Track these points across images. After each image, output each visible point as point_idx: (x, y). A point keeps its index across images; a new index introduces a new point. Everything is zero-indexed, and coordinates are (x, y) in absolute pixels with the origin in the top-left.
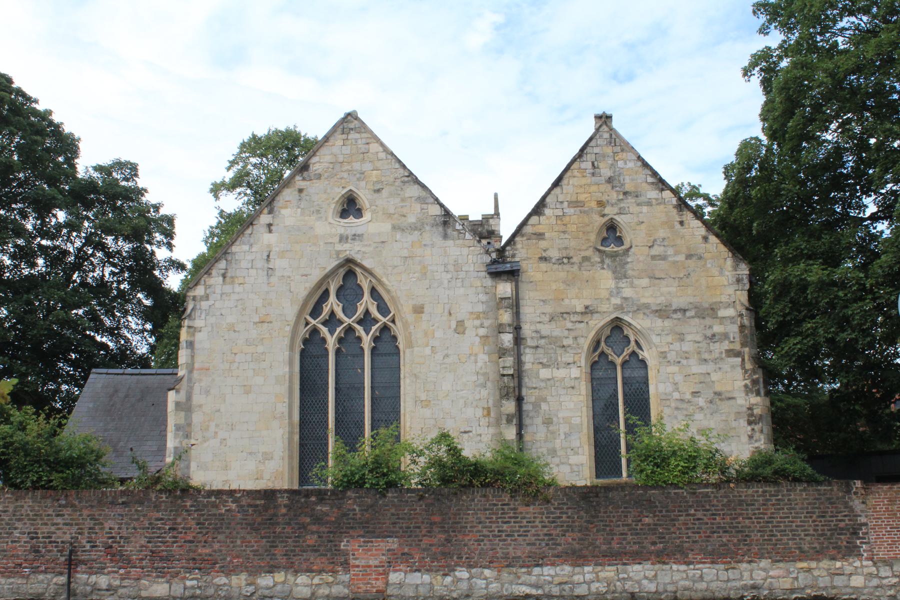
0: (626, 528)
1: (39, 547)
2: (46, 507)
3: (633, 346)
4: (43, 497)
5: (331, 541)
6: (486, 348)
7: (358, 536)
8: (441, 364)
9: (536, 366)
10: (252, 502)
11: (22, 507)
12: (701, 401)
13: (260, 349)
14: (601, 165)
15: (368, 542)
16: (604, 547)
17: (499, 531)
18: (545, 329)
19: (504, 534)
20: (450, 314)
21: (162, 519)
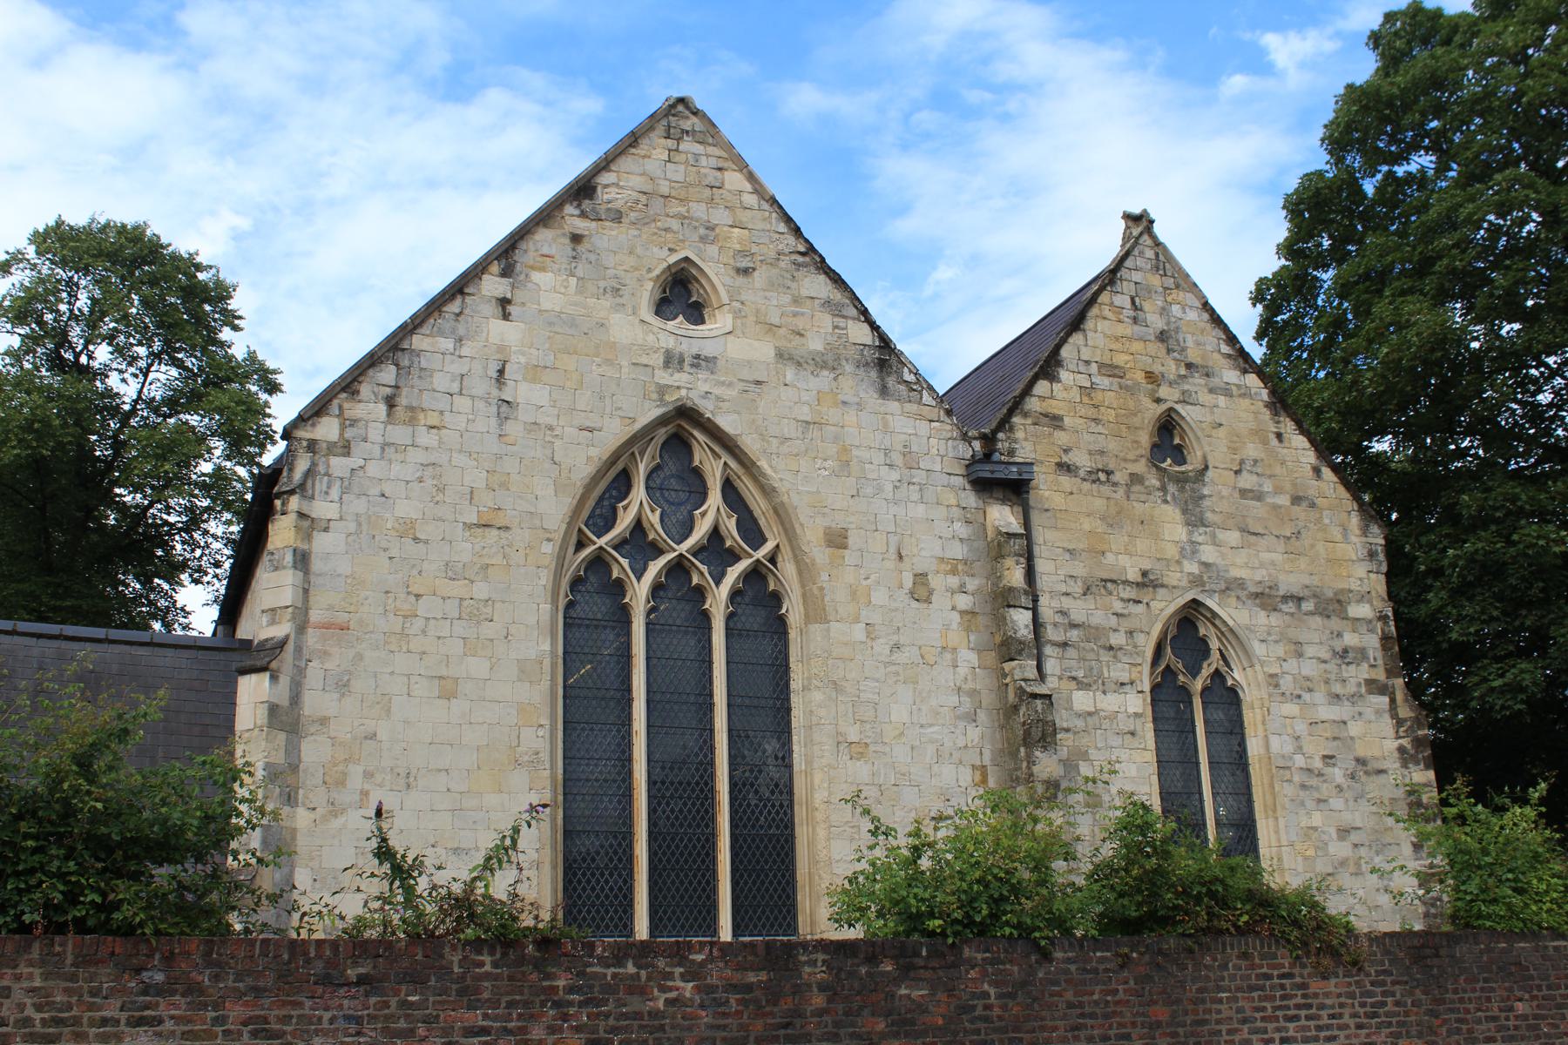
0: (1492, 1025)
2: (94, 993)
3: (1214, 662)
4: (83, 961)
6: (972, 638)
8: (887, 664)
9: (1067, 685)
10: (737, 977)
12: (1338, 774)
13: (481, 590)
14: (1147, 306)
18: (1080, 609)
20: (901, 557)
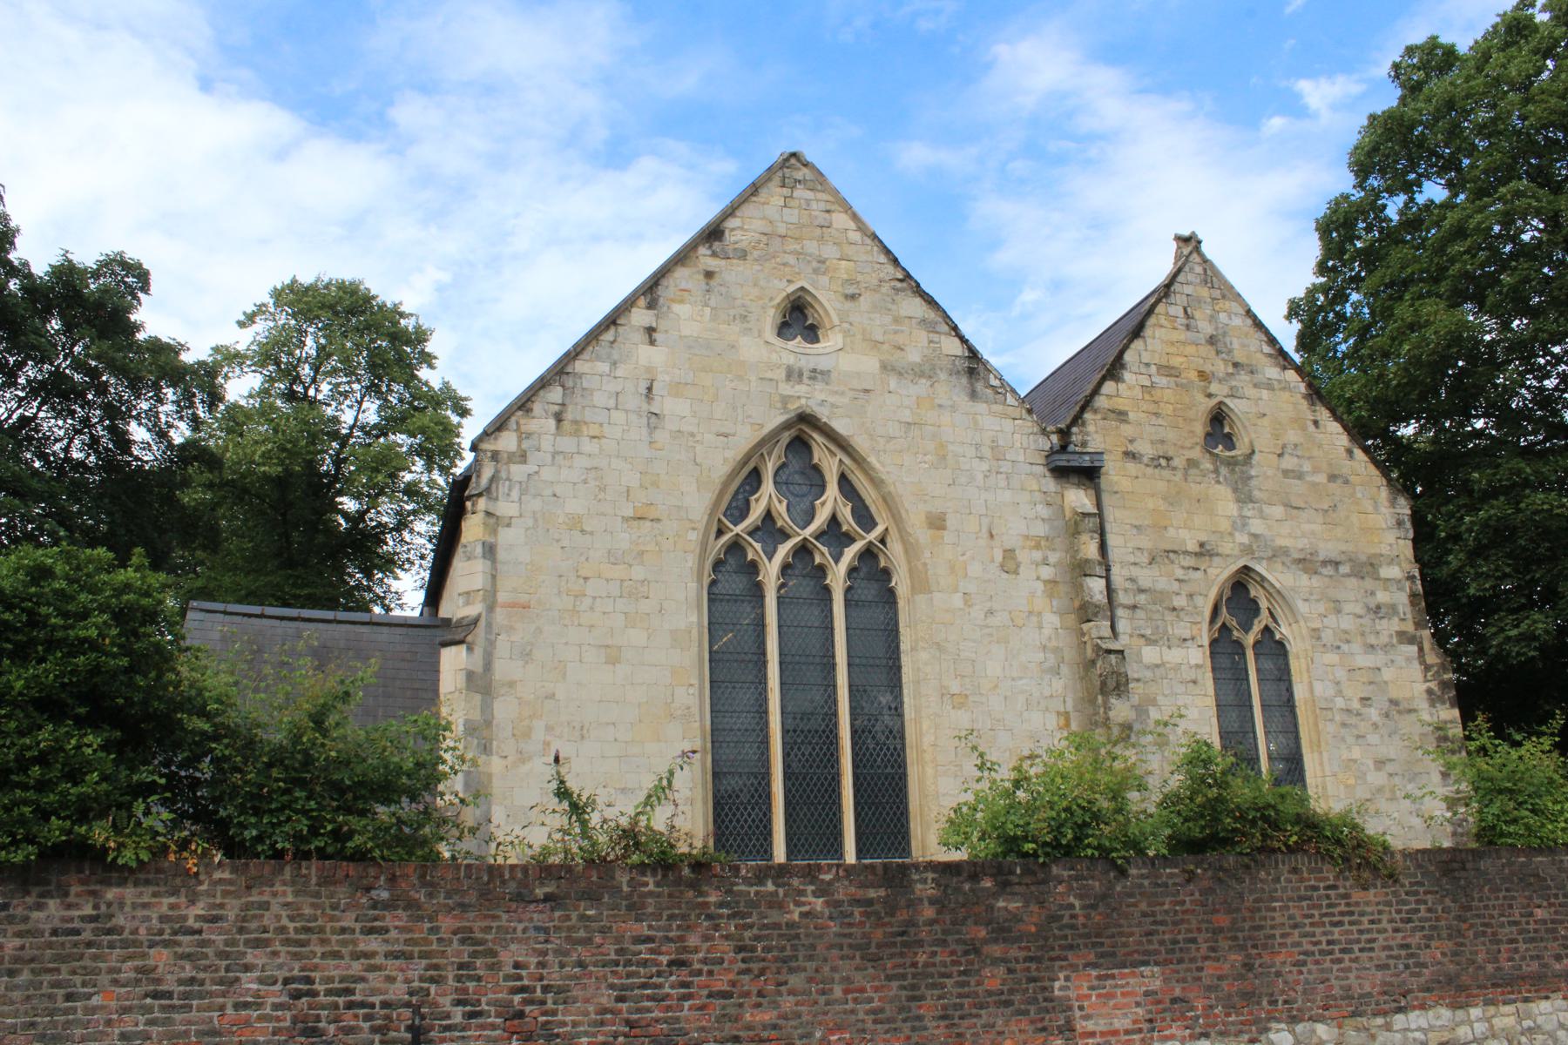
1: (318, 1019)
2: (334, 907)
4: (326, 881)
5: (1034, 980)
7: (1086, 966)
10: (860, 894)
11: (265, 906)
12: (1373, 714)
13: (638, 573)
14: (1197, 314)
15: (1108, 977)
16: (1490, 968)
17: (1329, 943)
18: (1146, 577)
19: (1337, 948)
20: (992, 536)
21: (649, 939)
